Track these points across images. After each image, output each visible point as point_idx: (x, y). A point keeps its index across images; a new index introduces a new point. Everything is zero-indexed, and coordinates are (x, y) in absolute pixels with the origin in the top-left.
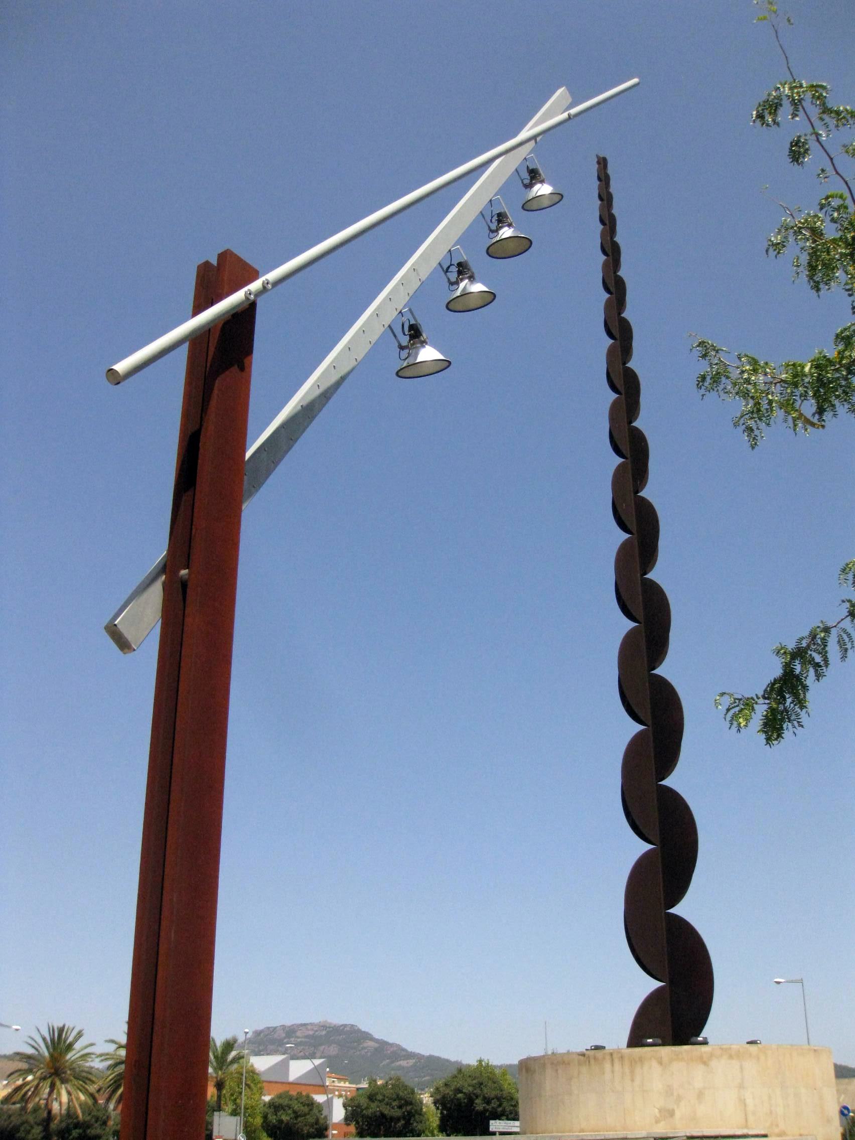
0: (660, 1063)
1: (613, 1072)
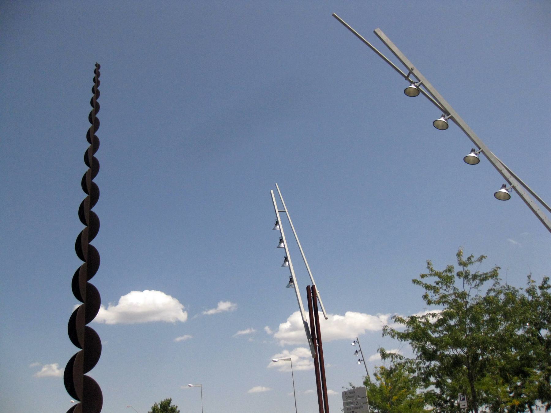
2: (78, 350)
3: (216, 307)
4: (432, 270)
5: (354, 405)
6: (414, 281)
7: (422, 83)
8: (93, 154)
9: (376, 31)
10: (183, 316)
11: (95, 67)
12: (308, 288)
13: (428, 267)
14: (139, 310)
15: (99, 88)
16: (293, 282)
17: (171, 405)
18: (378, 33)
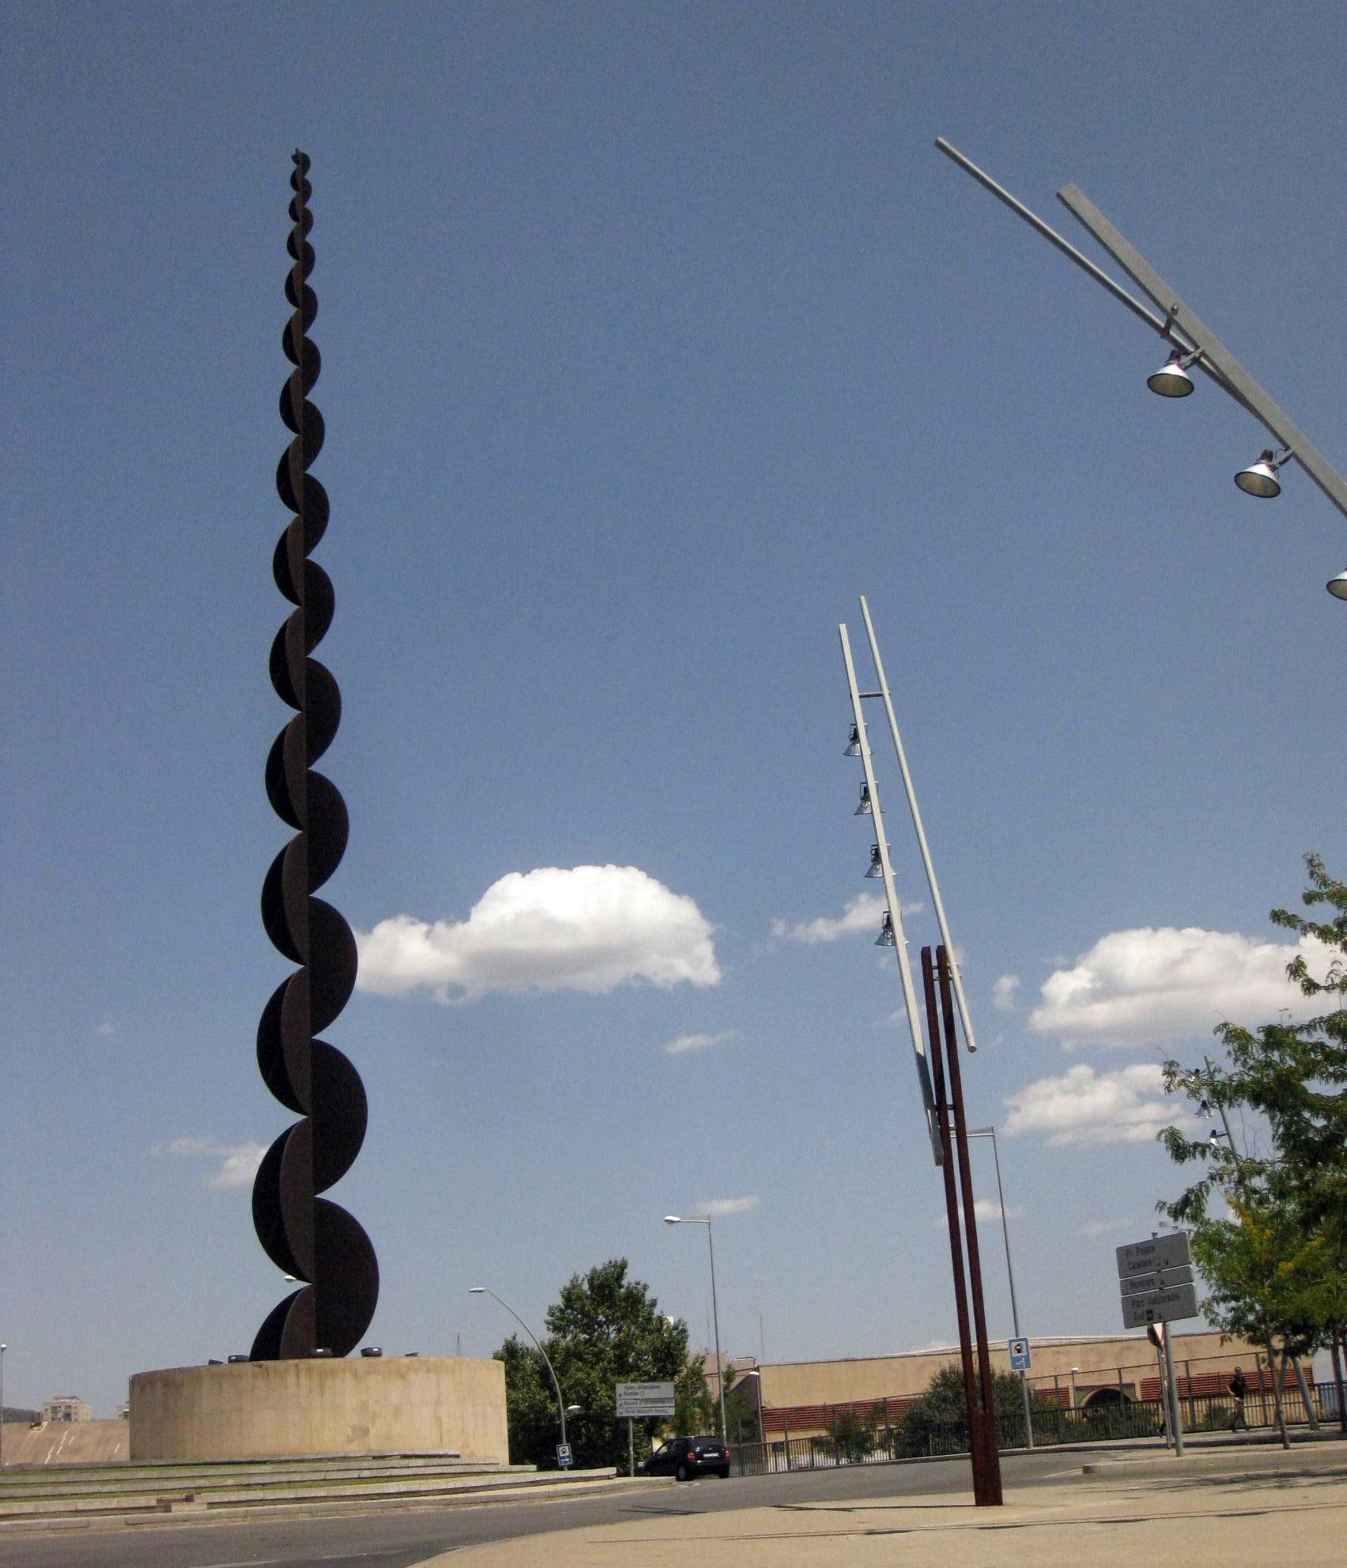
0: (355, 1375)
1: (298, 1384)
2: (297, 1118)
3: (839, 914)
4: (1324, 882)
5: (1153, 1291)
6: (1277, 916)
7: (1203, 354)
8: (306, 465)
9: (1063, 194)
10: (700, 966)
11: (293, 167)
12: (925, 954)
13: (1312, 874)
14: (561, 944)
15: (310, 238)
16: (892, 930)
17: (624, 1282)
18: (1071, 199)
